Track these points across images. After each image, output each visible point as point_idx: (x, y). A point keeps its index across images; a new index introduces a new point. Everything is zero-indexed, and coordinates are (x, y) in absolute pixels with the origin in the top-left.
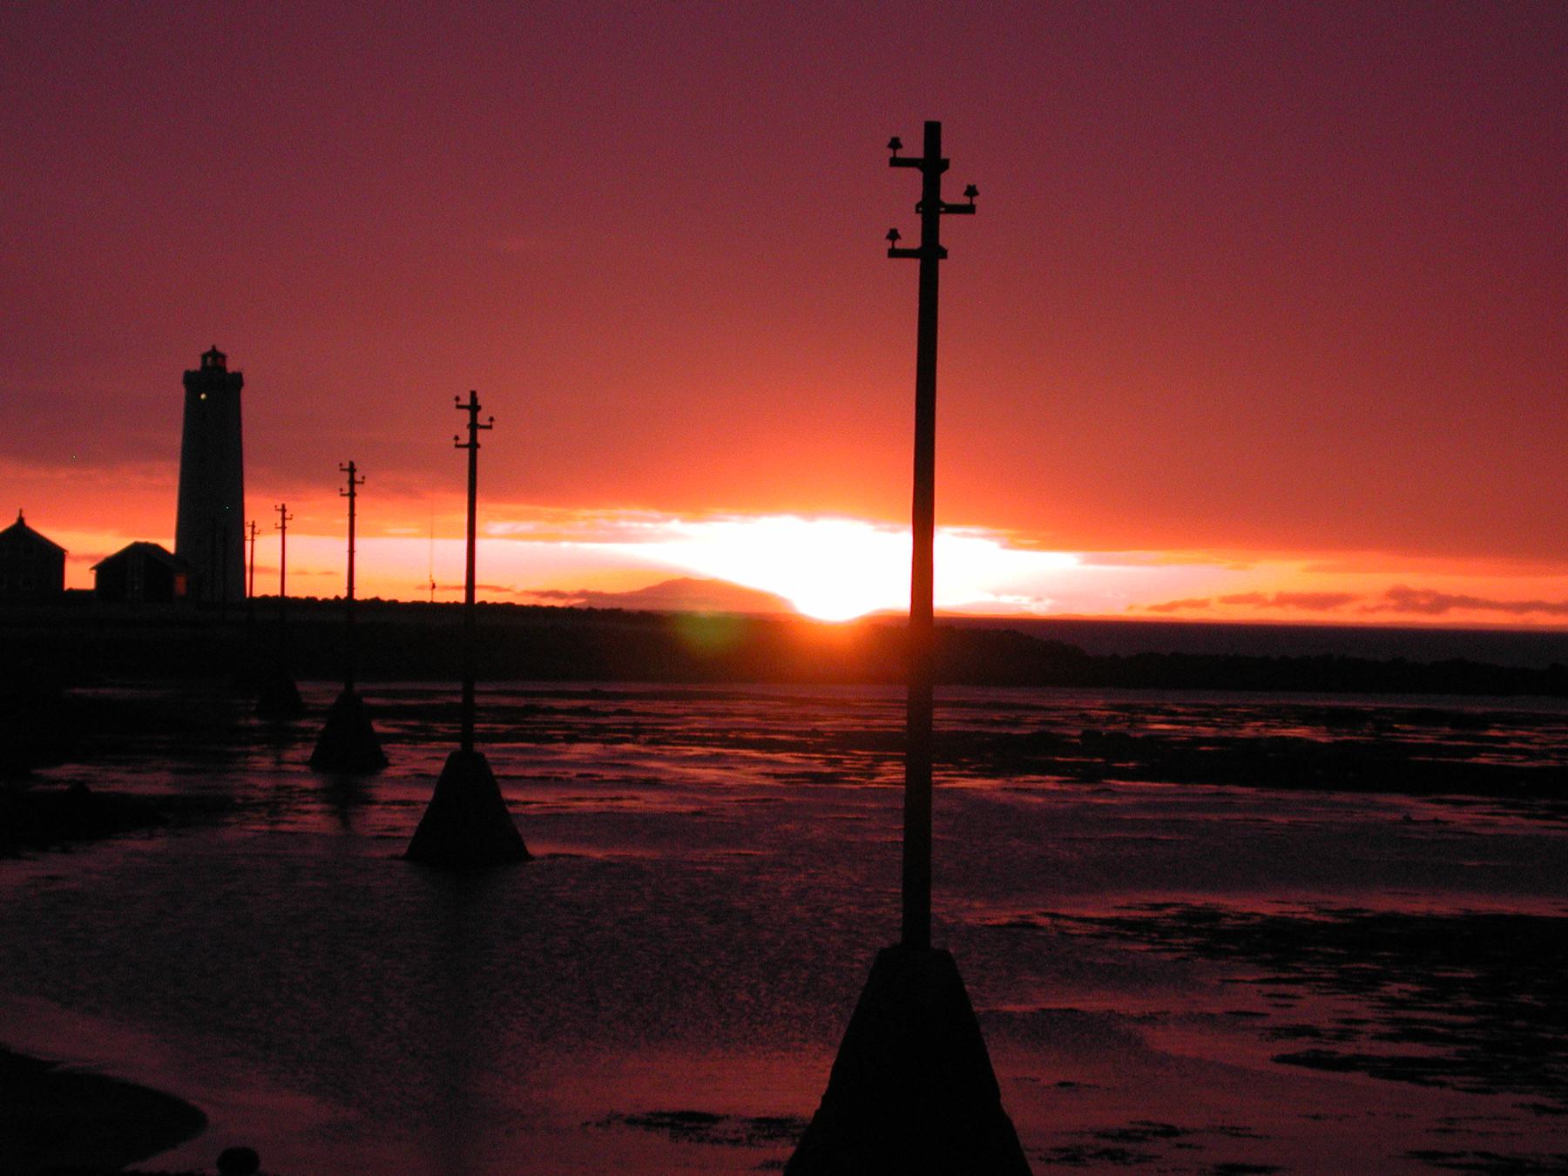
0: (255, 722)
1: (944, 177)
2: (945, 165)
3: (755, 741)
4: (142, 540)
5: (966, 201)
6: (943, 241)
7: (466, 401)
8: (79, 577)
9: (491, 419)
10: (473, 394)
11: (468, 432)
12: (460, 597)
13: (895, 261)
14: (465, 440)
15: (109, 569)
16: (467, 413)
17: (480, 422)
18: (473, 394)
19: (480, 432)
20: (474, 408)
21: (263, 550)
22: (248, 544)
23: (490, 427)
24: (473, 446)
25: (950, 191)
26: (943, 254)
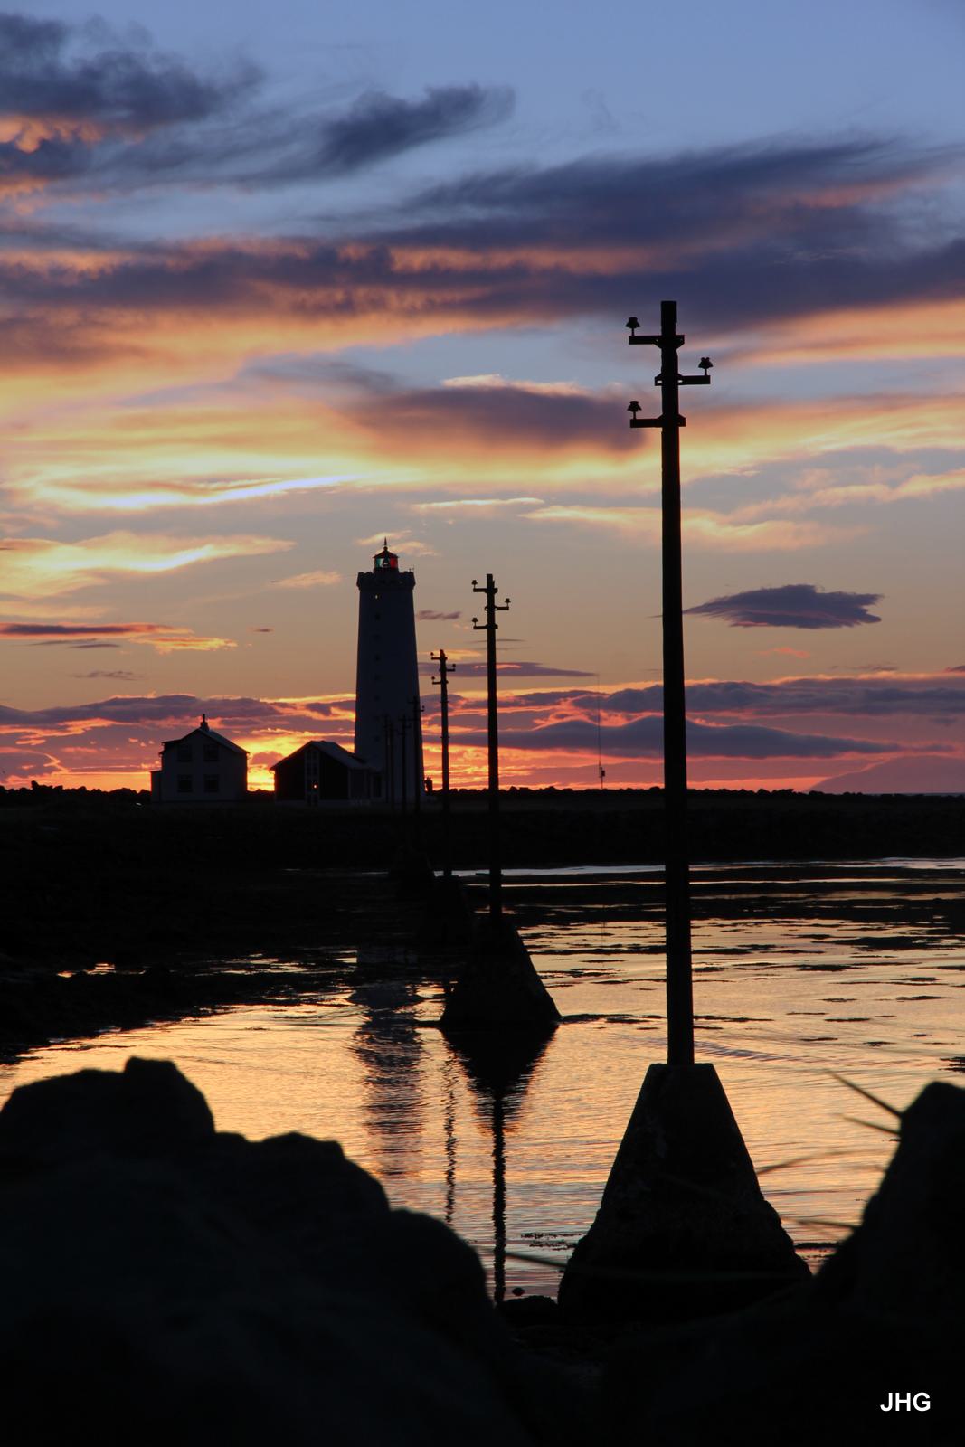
0: (26, 767)
1: (496, 595)
2: (496, 590)
3: (283, 1001)
4: (826, 760)
5: (505, 605)
6: (497, 622)
7: (483, 584)
8: (261, 780)
9: (508, 601)
10: (490, 577)
11: (485, 614)
12: (704, 933)
13: (477, 631)
14: (483, 621)
15: (284, 769)
16: (484, 596)
17: (497, 603)
18: (490, 577)
19: (497, 613)
20: (491, 590)
21: (663, 931)
22: (745, 724)
23: (507, 608)
24: (491, 627)
25: (499, 601)
26: (496, 627)
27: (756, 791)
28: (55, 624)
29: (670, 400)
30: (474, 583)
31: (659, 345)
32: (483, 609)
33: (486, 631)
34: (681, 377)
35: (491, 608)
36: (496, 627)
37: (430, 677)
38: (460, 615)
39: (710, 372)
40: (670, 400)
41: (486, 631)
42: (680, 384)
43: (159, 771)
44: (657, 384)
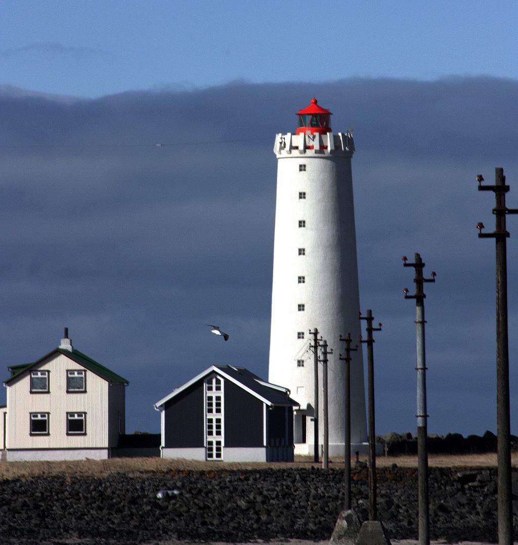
1: (507, 195)
7: (491, 180)
9: (434, 274)
14: (491, 227)
19: (425, 285)
23: (433, 281)
24: (501, 236)
26: (508, 235)
27: (465, 436)
28: (343, 407)
29: (501, 223)
30: (405, 259)
31: (414, 267)
32: (426, 265)
33: (494, 240)
34: (508, 210)
35: (420, 281)
36: (508, 235)
37: (222, 458)
38: (479, 174)
39: (435, 277)
40: (501, 223)
41: (494, 240)
42: (507, 214)
43: (64, 354)
44: (493, 213)
